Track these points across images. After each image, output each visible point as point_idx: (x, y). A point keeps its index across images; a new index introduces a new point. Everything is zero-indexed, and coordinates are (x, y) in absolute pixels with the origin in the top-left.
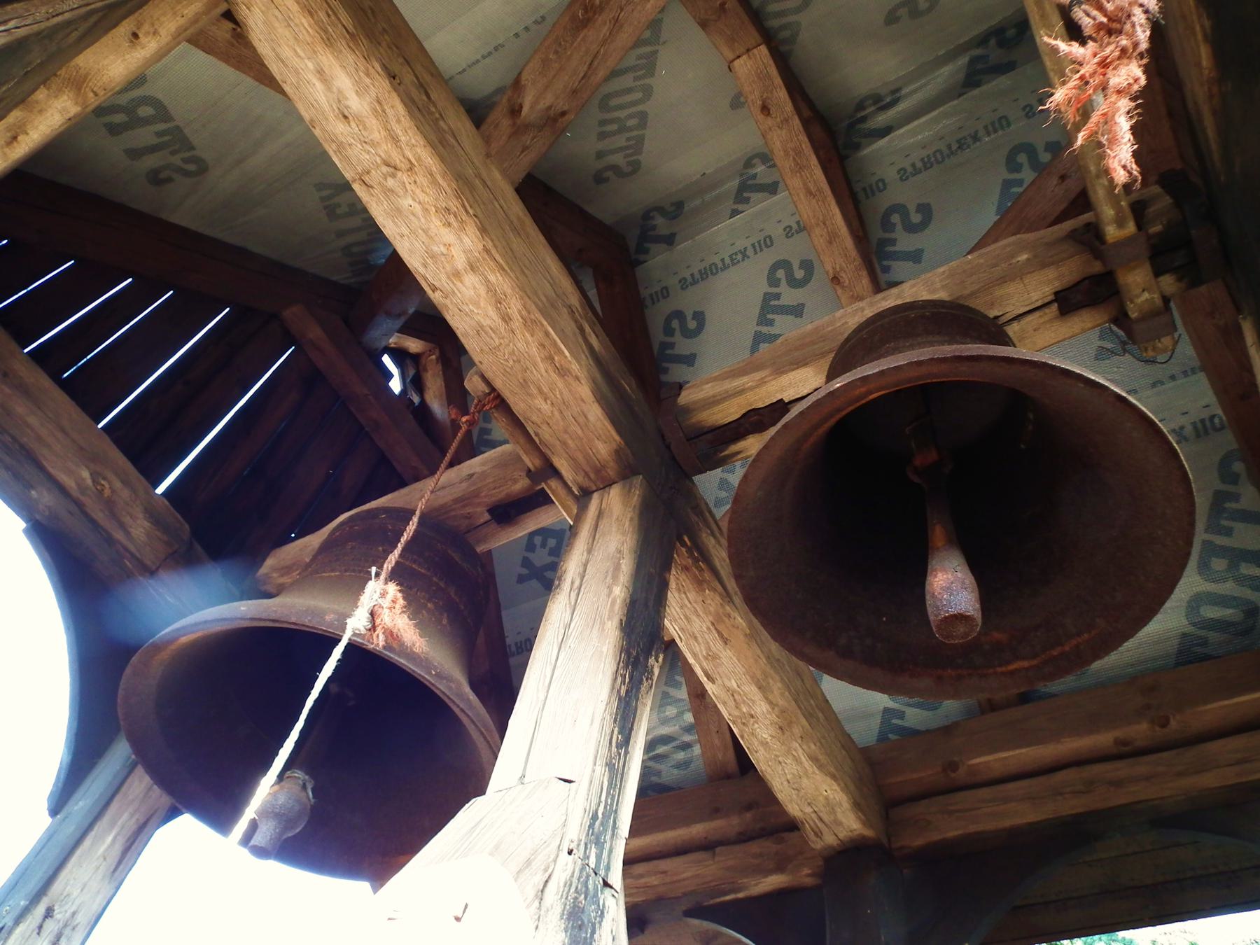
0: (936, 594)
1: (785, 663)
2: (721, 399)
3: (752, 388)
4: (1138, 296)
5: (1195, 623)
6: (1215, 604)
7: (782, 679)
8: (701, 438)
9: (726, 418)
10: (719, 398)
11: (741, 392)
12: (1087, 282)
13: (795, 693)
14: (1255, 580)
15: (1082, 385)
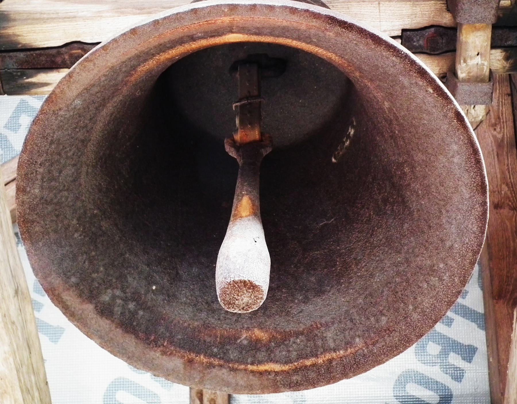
0: (231, 257)
1: (19, 328)
2: (48, 19)
3: (85, 19)
4: (471, 58)
5: (399, 396)
6: (420, 383)
7: (11, 343)
8: (11, 54)
9: (46, 41)
10: (45, 16)
11: (72, 18)
12: (433, 30)
13: (19, 362)
14: (457, 370)
15: (431, 91)
